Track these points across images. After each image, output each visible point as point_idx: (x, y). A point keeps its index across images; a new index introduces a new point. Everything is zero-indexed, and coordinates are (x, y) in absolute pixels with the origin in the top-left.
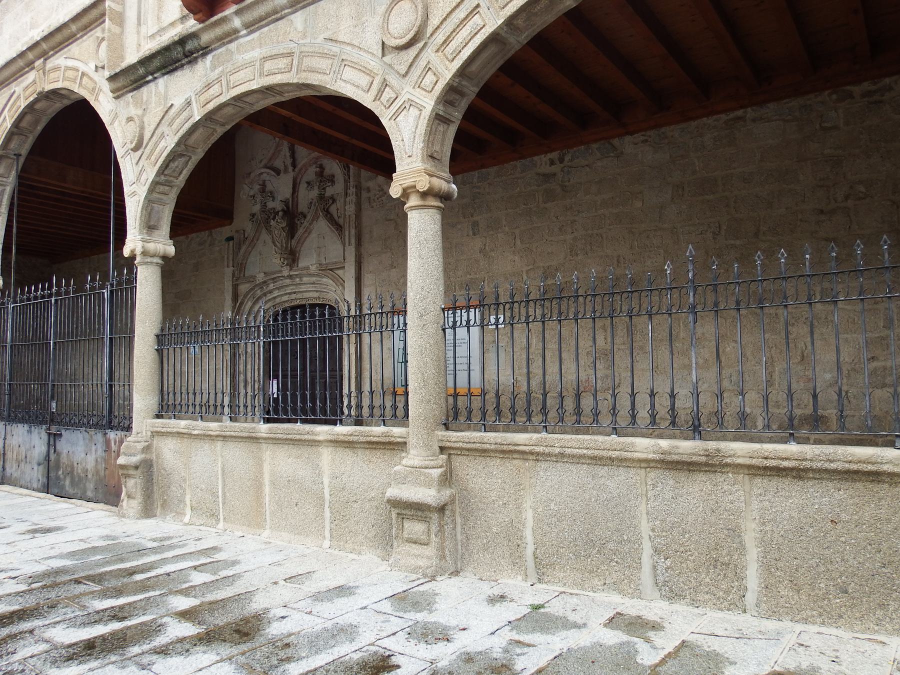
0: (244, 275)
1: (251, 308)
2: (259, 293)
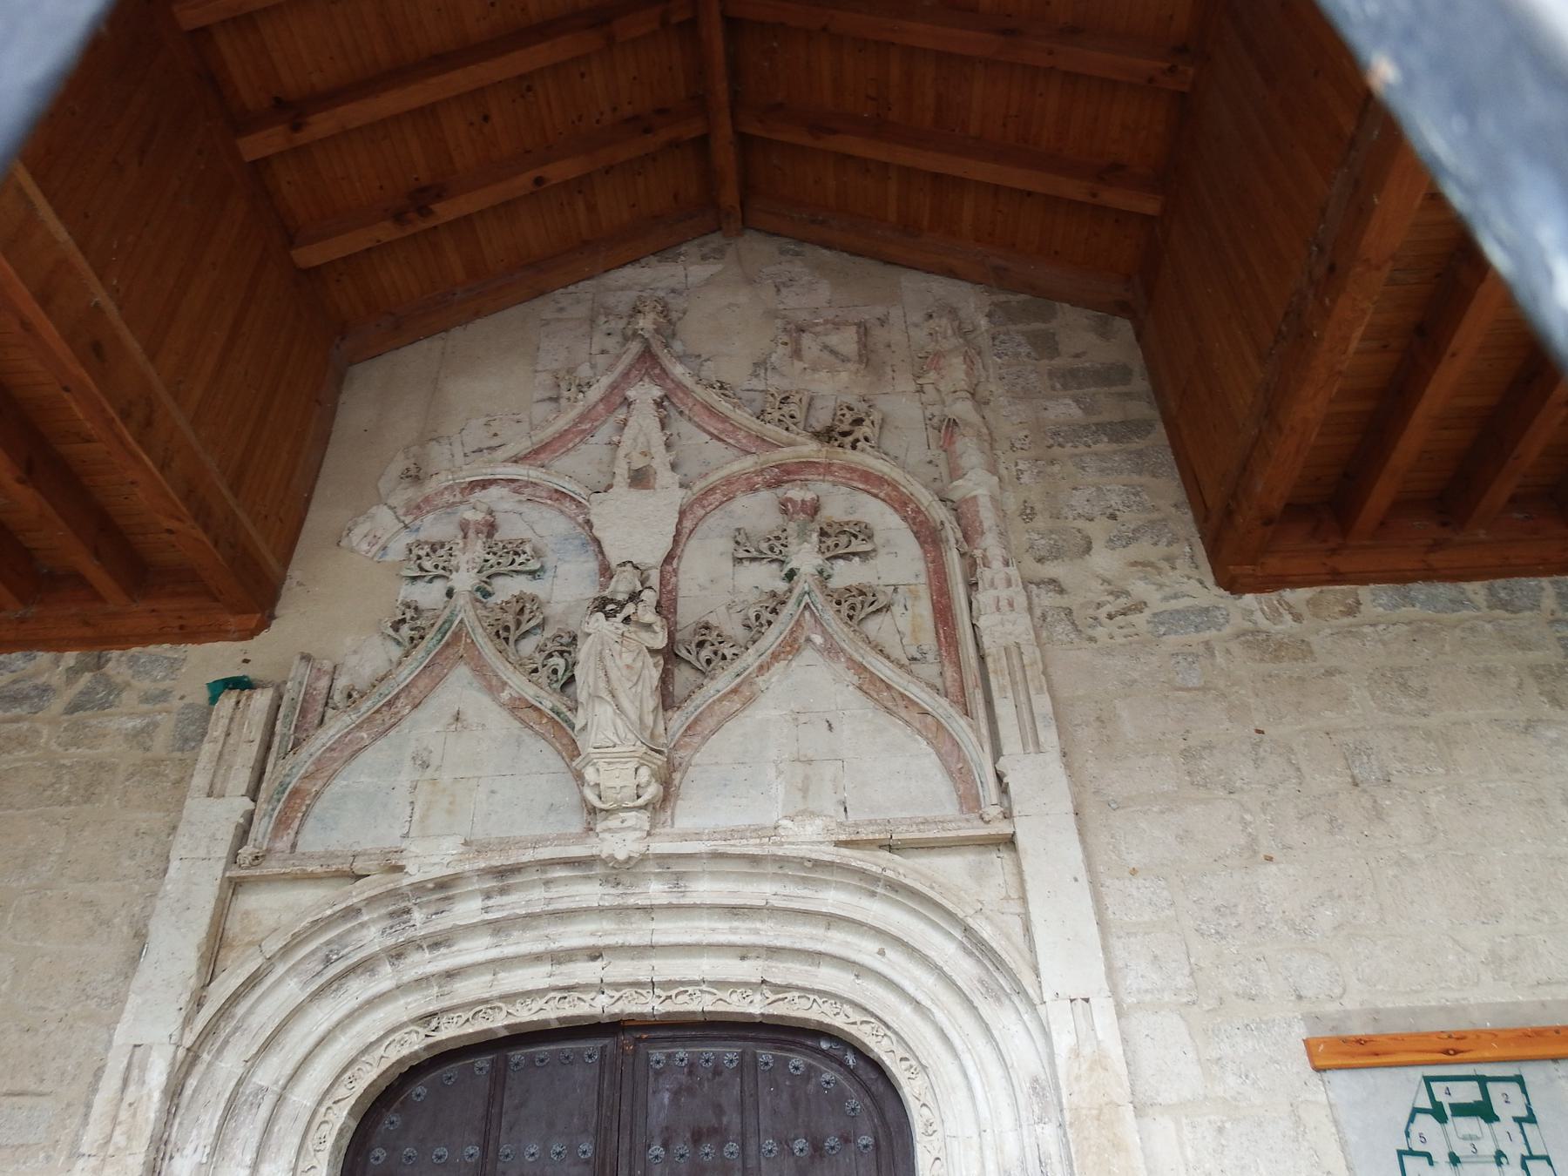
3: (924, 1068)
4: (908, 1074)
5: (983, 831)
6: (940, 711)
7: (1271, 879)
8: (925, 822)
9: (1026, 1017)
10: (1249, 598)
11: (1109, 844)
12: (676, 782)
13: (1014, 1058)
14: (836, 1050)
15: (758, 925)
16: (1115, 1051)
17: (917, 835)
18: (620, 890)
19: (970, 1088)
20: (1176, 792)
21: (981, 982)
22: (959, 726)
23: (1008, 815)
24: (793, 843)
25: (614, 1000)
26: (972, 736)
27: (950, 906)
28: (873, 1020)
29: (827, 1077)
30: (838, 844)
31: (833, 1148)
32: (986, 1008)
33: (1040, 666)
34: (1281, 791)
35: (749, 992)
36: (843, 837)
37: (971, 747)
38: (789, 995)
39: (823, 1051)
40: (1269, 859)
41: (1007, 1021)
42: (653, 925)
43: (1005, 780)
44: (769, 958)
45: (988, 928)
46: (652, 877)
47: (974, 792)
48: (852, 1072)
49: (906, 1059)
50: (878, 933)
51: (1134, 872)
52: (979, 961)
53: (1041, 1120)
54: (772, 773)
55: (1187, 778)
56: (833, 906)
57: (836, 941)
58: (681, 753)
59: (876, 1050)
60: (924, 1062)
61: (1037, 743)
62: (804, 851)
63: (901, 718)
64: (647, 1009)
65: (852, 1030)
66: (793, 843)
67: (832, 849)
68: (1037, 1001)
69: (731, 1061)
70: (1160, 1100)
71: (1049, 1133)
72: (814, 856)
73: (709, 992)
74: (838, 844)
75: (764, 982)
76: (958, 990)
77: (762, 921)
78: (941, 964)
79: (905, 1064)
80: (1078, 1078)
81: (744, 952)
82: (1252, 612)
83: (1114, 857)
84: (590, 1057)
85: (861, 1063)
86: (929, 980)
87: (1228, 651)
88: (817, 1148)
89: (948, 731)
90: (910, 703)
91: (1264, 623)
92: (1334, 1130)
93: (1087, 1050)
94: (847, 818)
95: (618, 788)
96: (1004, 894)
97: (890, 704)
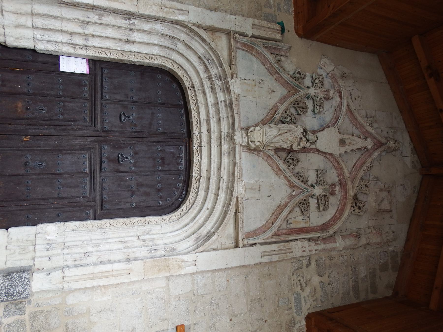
0: (238, 48)
1: (195, 53)
2: (214, 71)
3: (178, 219)
4: (177, 215)
5: (240, 239)
6: (273, 228)
7: (225, 320)
8: (243, 223)
9: (191, 248)
10: (304, 323)
11: (236, 274)
12: (254, 153)
13: (181, 244)
14: (183, 196)
15: (216, 175)
16: (183, 272)
17: (239, 220)
18: (226, 137)
19: (173, 232)
20: (250, 295)
21: (200, 236)
22: (269, 233)
23: (244, 246)
24: (238, 185)
25: (197, 136)
26: (266, 237)
27: (221, 228)
28: (190, 206)
29: (176, 193)
30: (237, 198)
31: (159, 194)
32: (193, 237)
33: (286, 258)
34: (249, 325)
35: (198, 173)
36: (239, 199)
37: (263, 236)
38: (197, 183)
39: (183, 192)
40: (231, 320)
41: (190, 242)
42: (216, 146)
43: (254, 246)
44: (207, 178)
45: (214, 239)
46: (229, 146)
47: (251, 236)
48: (177, 200)
49: (181, 215)
50: (213, 208)
51: (228, 281)
52: (206, 236)
53: (165, 250)
54: (257, 179)
55: (253, 299)
56: (221, 196)
57: (211, 196)
58: (262, 154)
59: (183, 206)
60: (180, 219)
61: (264, 256)
62: (236, 188)
63: (271, 217)
64: (194, 145)
65: (188, 200)
66: (238, 185)
67: (236, 196)
68: (196, 251)
69: (181, 168)
70: (170, 283)
71: (162, 252)
72: (234, 191)
73: (198, 162)
74: (237, 198)
75: (201, 176)
76: (198, 230)
77: (217, 176)
78: (205, 225)
79: (179, 214)
80: (176, 261)
81: (209, 171)
82: (300, 323)
83: (232, 275)
84: (182, 130)
85: (179, 203)
86: (201, 221)
87: (289, 314)
88: (159, 190)
89: (268, 230)
90: (276, 220)
91: (297, 326)
92: (162, 330)
93: (183, 264)
94: (244, 200)
95: (254, 136)
96: (223, 243)
97: (275, 214)
